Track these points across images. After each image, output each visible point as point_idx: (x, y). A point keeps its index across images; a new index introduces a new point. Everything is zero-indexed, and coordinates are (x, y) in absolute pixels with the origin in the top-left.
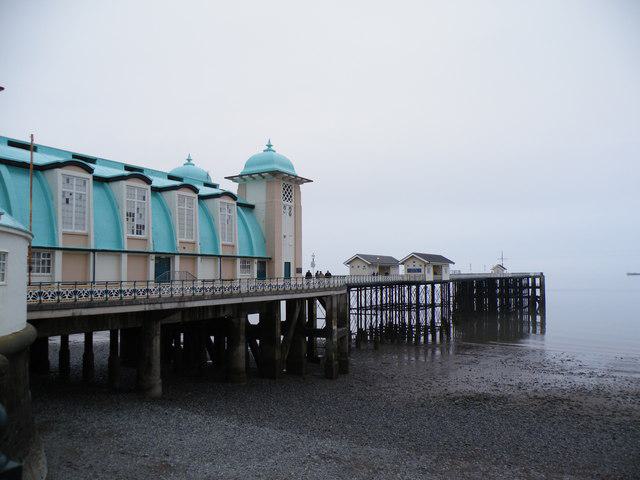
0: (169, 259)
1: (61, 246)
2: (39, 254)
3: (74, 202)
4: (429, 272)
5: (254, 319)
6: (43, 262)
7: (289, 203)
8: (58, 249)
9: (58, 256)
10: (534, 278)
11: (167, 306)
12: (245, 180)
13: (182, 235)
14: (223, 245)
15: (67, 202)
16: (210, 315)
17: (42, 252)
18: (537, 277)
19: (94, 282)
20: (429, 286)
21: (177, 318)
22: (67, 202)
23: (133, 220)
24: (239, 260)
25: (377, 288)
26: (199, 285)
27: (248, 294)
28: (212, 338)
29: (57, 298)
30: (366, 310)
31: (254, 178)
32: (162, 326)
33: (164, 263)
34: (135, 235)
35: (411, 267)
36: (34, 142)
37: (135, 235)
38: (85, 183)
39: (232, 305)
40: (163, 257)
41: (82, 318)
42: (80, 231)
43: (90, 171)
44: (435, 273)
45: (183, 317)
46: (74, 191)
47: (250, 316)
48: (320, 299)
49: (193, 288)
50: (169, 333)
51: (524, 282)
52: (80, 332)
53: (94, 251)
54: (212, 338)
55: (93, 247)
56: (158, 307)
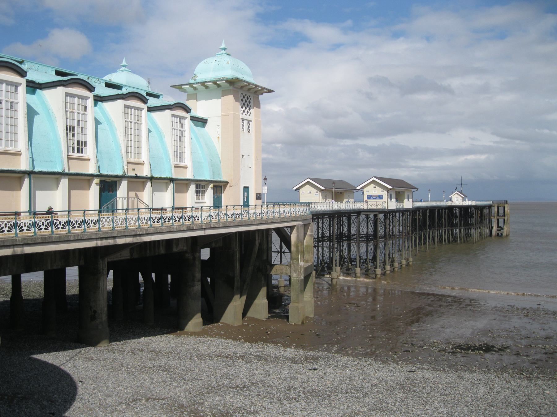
0: (115, 182)
5: (205, 254)
11: (121, 241)
16: (162, 251)
23: (73, 135)
26: (145, 214)
31: (207, 87)
33: (108, 186)
34: (76, 154)
37: (76, 154)
40: (108, 180)
43: (22, 73)
45: (131, 254)
47: (76, 268)
49: (138, 219)
50: (445, 209)
52: (9, 274)
56: (111, 242)
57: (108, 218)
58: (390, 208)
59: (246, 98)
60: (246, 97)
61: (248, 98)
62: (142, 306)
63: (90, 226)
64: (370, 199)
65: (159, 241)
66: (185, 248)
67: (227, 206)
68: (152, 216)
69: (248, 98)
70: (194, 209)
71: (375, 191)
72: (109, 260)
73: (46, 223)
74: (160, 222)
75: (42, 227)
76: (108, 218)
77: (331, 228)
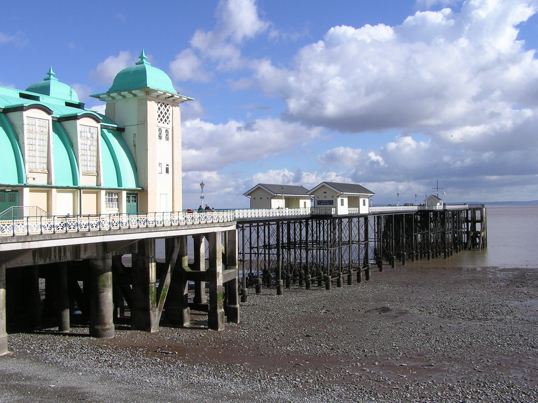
4: (342, 204)
7: (165, 125)
10: (474, 211)
12: (113, 98)
16: (69, 257)
18: (477, 209)
20: (362, 220)
21: (28, 261)
24: (103, 192)
25: (258, 226)
27: (42, 237)
28: (81, 283)
29: (76, 228)
30: (270, 249)
32: (8, 270)
35: (322, 198)
36: (361, 213)
39: (97, 244)
44: (350, 206)
48: (207, 235)
51: (463, 215)
52: (90, 332)
54: (81, 283)
57: (8, 225)
58: (361, 213)
59: (164, 120)
60: (163, 121)
61: (161, 120)
62: (418, 216)
63: (19, 231)
64: (320, 204)
65: (65, 247)
66: (95, 255)
67: (28, 217)
68: (90, 222)
69: (161, 120)
70: (56, 218)
71: (325, 197)
72: (9, 267)
73: (49, 225)
74: (65, 228)
75: (33, 229)
76: (8, 225)
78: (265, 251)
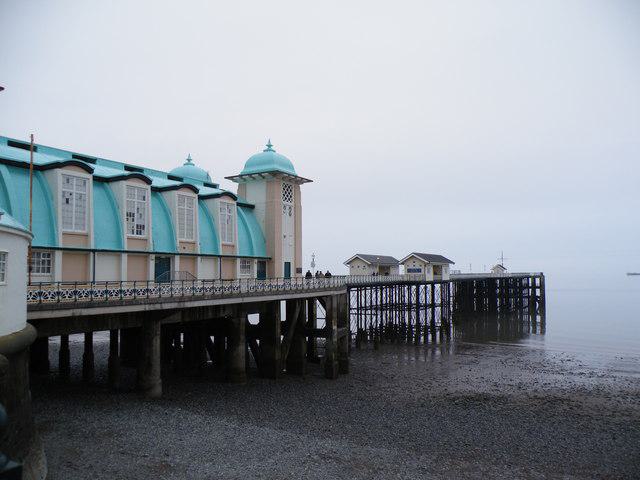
0: (169, 259)
1: (61, 246)
2: (39, 254)
3: (74, 202)
4: (429, 272)
5: (254, 319)
6: (43, 262)
7: (289, 203)
8: (58, 249)
9: (58, 256)
10: (534, 278)
11: (167, 306)
12: (245, 180)
13: (182, 235)
14: (223, 245)
15: (67, 202)
16: (210, 315)
17: (42, 252)
18: (537, 277)
19: (94, 282)
20: (429, 286)
21: (177, 318)
22: (67, 202)
23: (133, 220)
24: (239, 260)
25: (377, 288)
26: (199, 285)
27: (248, 294)
28: (212, 338)
29: (57, 298)
30: (366, 310)
31: (254, 178)
32: (162, 326)
33: (164, 263)
34: (135, 235)
35: (411, 267)
37: (135, 235)
38: (85, 183)
39: (232, 305)
40: (163, 257)
41: (82, 318)
42: (80, 231)
43: (90, 171)
44: (435, 273)
45: (183, 317)
46: (74, 191)
47: (250, 316)
48: (320, 299)
49: (193, 288)
50: (169, 333)
51: (524, 282)
52: (80, 332)
53: (94, 251)
54: (212, 338)
55: (93, 247)
56: (158, 307)
77: (24, 234)
78: (534, 319)
